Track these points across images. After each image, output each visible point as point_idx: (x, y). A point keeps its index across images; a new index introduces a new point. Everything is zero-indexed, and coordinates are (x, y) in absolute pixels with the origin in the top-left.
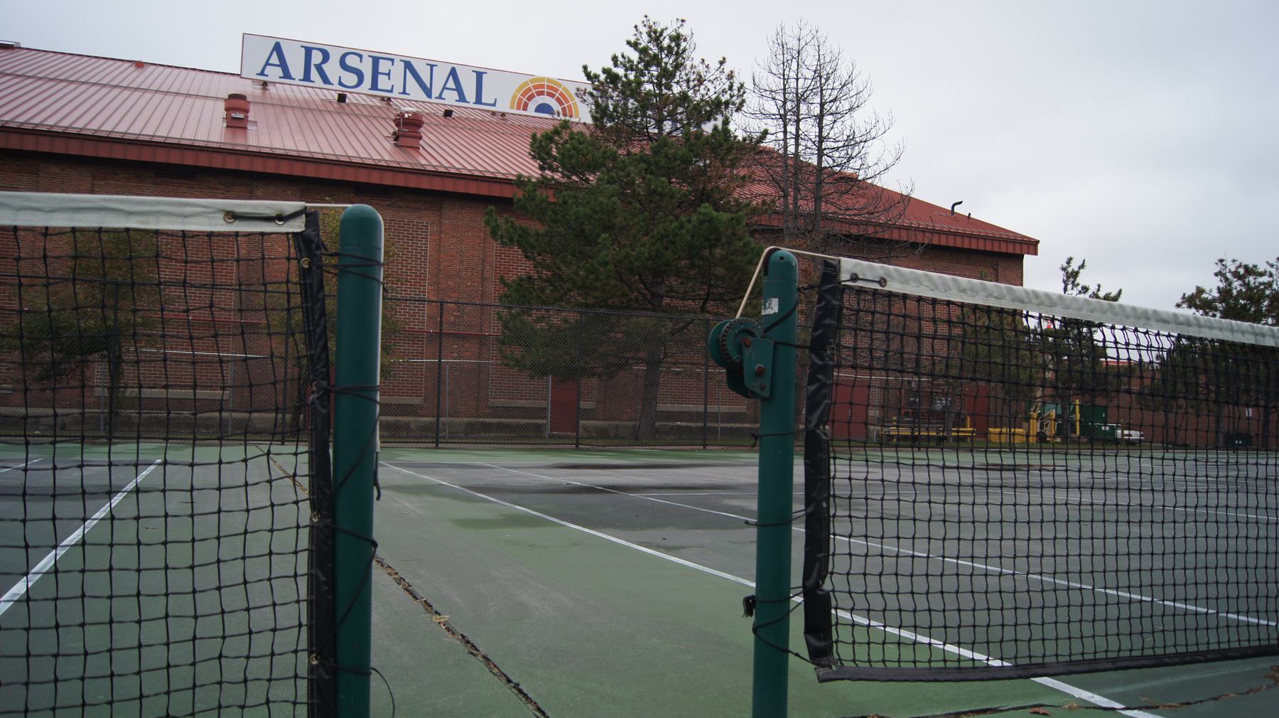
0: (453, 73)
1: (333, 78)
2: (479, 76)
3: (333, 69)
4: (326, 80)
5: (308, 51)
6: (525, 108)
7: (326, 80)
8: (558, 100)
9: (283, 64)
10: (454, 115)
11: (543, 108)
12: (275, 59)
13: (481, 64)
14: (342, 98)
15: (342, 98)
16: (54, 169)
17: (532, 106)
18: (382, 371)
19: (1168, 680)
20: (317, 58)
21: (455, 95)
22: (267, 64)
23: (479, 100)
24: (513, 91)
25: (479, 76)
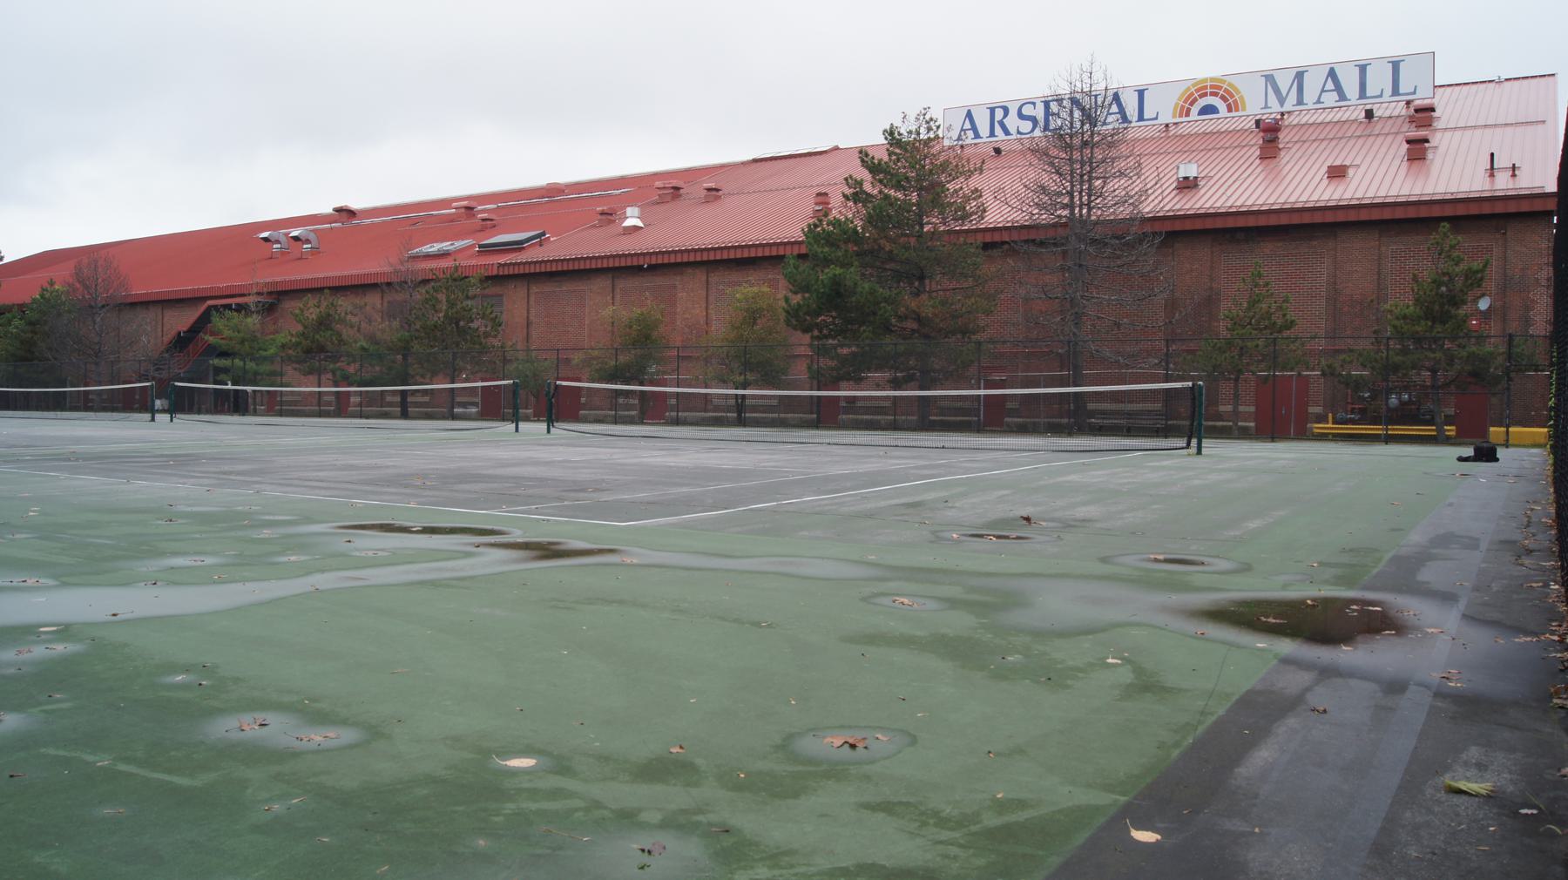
0: (969, 115)
1: (1013, 130)
2: (1141, 93)
3: (1012, 122)
4: (1007, 133)
5: (992, 110)
6: (1187, 115)
7: (1007, 133)
8: (1201, 96)
9: (1338, 88)
10: (1377, 113)
11: (1209, 110)
12: (1330, 85)
13: (1140, 81)
14: (1369, 114)
15: (1369, 114)
16: (690, 271)
17: (1195, 109)
18: (1167, 381)
19: (685, 490)
20: (999, 114)
21: (1335, 95)
22: (1323, 91)
23: (1141, 118)
24: (1175, 100)
25: (1141, 93)
